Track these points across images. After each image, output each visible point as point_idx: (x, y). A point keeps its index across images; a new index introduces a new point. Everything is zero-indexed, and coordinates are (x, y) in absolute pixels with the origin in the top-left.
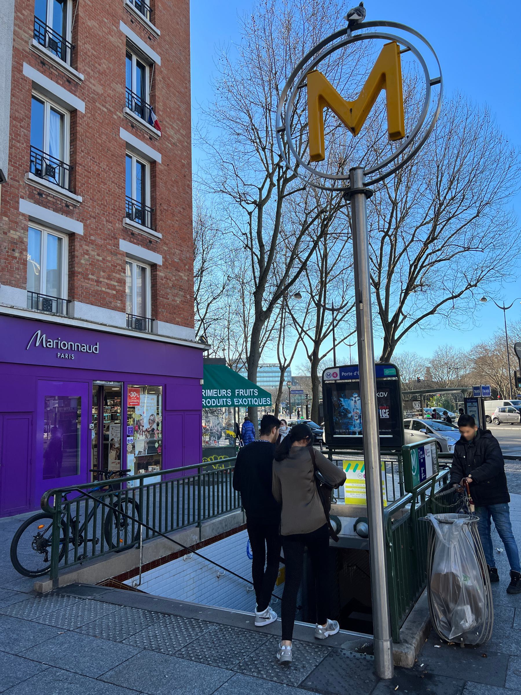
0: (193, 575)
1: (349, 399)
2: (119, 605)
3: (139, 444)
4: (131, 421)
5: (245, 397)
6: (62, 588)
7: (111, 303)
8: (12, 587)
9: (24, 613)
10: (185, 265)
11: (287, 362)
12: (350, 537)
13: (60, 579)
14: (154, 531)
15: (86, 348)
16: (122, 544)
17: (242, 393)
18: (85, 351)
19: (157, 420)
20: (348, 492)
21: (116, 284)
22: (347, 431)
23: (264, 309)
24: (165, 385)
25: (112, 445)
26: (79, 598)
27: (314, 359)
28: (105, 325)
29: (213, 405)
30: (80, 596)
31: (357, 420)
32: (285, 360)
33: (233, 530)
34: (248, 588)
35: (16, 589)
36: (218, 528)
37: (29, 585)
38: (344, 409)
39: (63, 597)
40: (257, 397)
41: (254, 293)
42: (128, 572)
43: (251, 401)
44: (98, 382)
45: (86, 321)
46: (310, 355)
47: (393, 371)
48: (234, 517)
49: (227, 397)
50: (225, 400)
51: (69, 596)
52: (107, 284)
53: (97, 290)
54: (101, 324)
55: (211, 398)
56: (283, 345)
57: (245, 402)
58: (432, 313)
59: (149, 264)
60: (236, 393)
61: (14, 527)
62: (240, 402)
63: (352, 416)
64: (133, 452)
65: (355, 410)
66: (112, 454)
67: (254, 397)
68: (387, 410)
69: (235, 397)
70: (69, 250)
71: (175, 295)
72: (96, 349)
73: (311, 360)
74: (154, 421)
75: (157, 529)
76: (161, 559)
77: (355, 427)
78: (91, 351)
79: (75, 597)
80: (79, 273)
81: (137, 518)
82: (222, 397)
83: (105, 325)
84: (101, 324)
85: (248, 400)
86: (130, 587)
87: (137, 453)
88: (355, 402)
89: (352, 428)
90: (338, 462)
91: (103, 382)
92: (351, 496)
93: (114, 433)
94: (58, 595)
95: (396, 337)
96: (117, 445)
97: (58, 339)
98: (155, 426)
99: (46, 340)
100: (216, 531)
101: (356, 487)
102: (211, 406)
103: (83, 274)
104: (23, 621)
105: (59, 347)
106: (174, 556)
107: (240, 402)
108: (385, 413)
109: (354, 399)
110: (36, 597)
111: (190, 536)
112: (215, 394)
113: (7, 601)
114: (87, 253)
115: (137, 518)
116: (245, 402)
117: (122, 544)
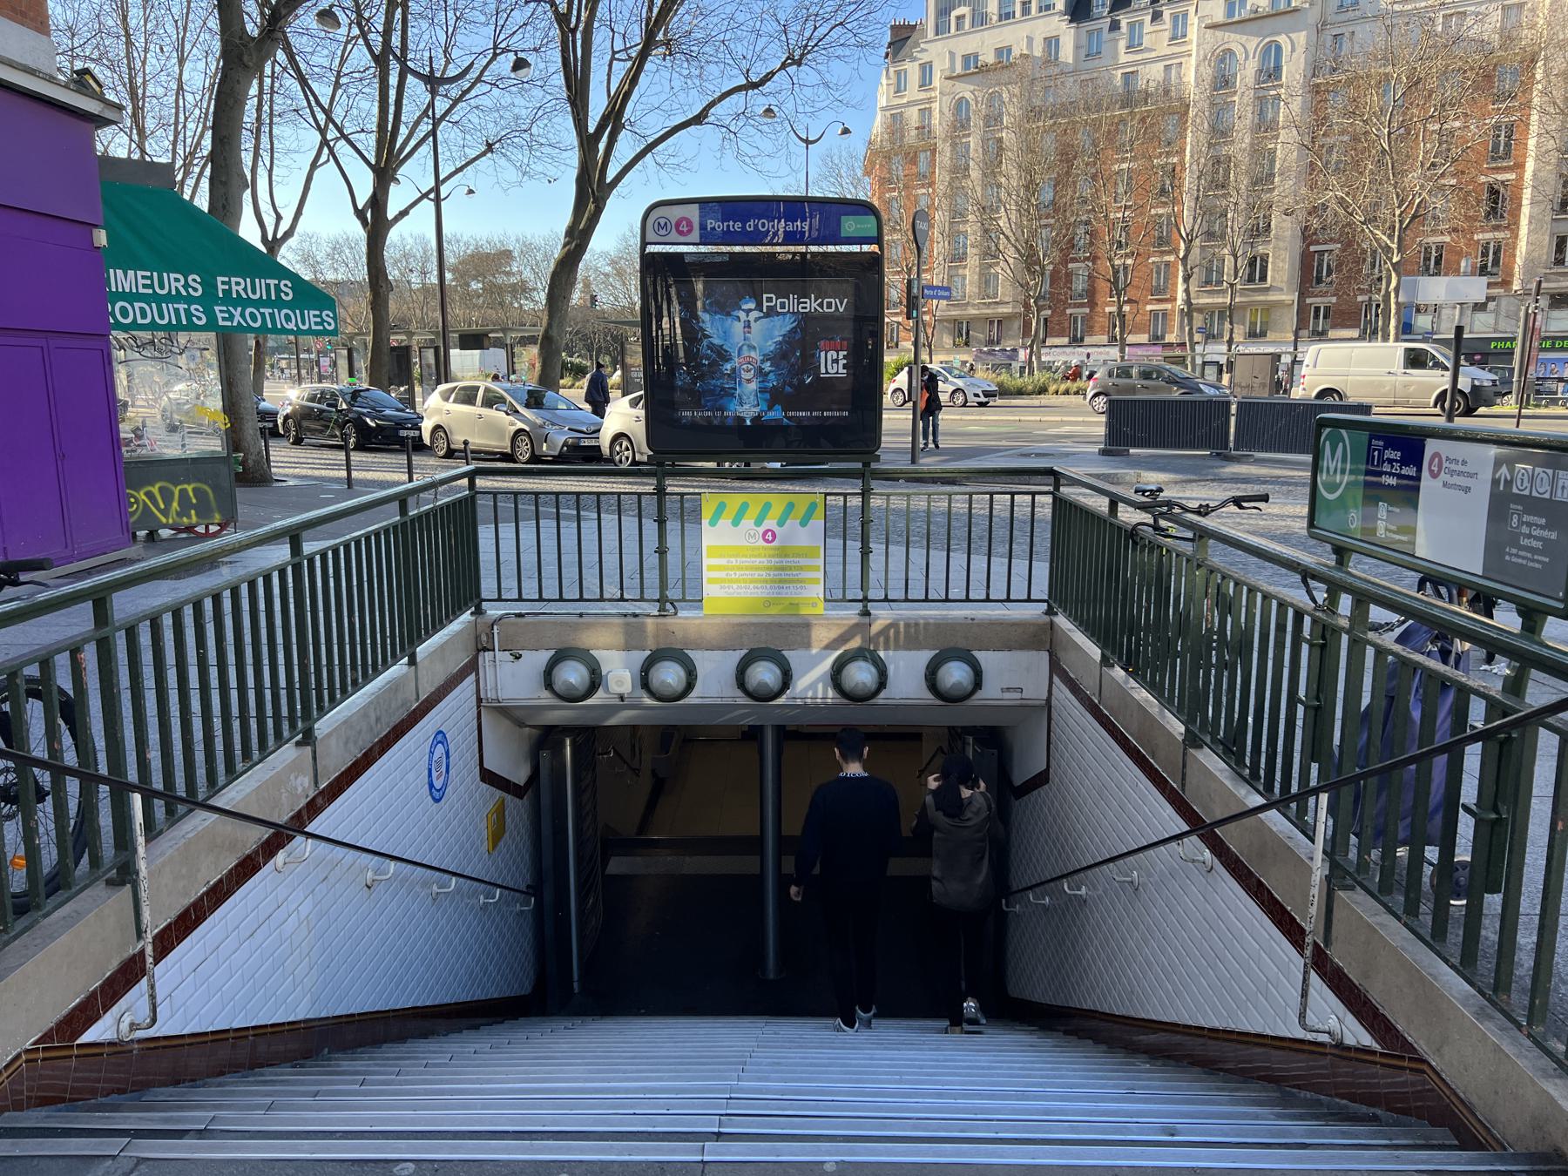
1: (728, 314)
5: (249, 302)
11: (284, 226)
12: (719, 701)
17: (240, 288)
20: (712, 581)
22: (719, 414)
27: (375, 219)
29: (140, 321)
31: (749, 381)
32: (279, 218)
33: (395, 728)
34: (435, 888)
36: (360, 732)
38: (711, 347)
40: (290, 305)
42: (94, 992)
43: (272, 315)
46: (360, 207)
49: (189, 300)
50: (182, 307)
55: (132, 297)
56: (270, 171)
57: (254, 319)
60: (221, 287)
62: (237, 318)
63: (734, 370)
65: (745, 352)
67: (279, 304)
68: (842, 354)
69: (216, 300)
73: (364, 222)
76: (207, 893)
77: (741, 404)
81: (70, 758)
82: (169, 298)
85: (263, 315)
86: (111, 1044)
88: (748, 325)
89: (732, 407)
90: (602, 498)
92: (722, 594)
100: (355, 743)
101: (740, 568)
102: (135, 325)
106: (247, 868)
107: (237, 318)
108: (836, 361)
109: (742, 315)
111: (272, 780)
112: (144, 286)
115: (70, 758)
116: (255, 320)
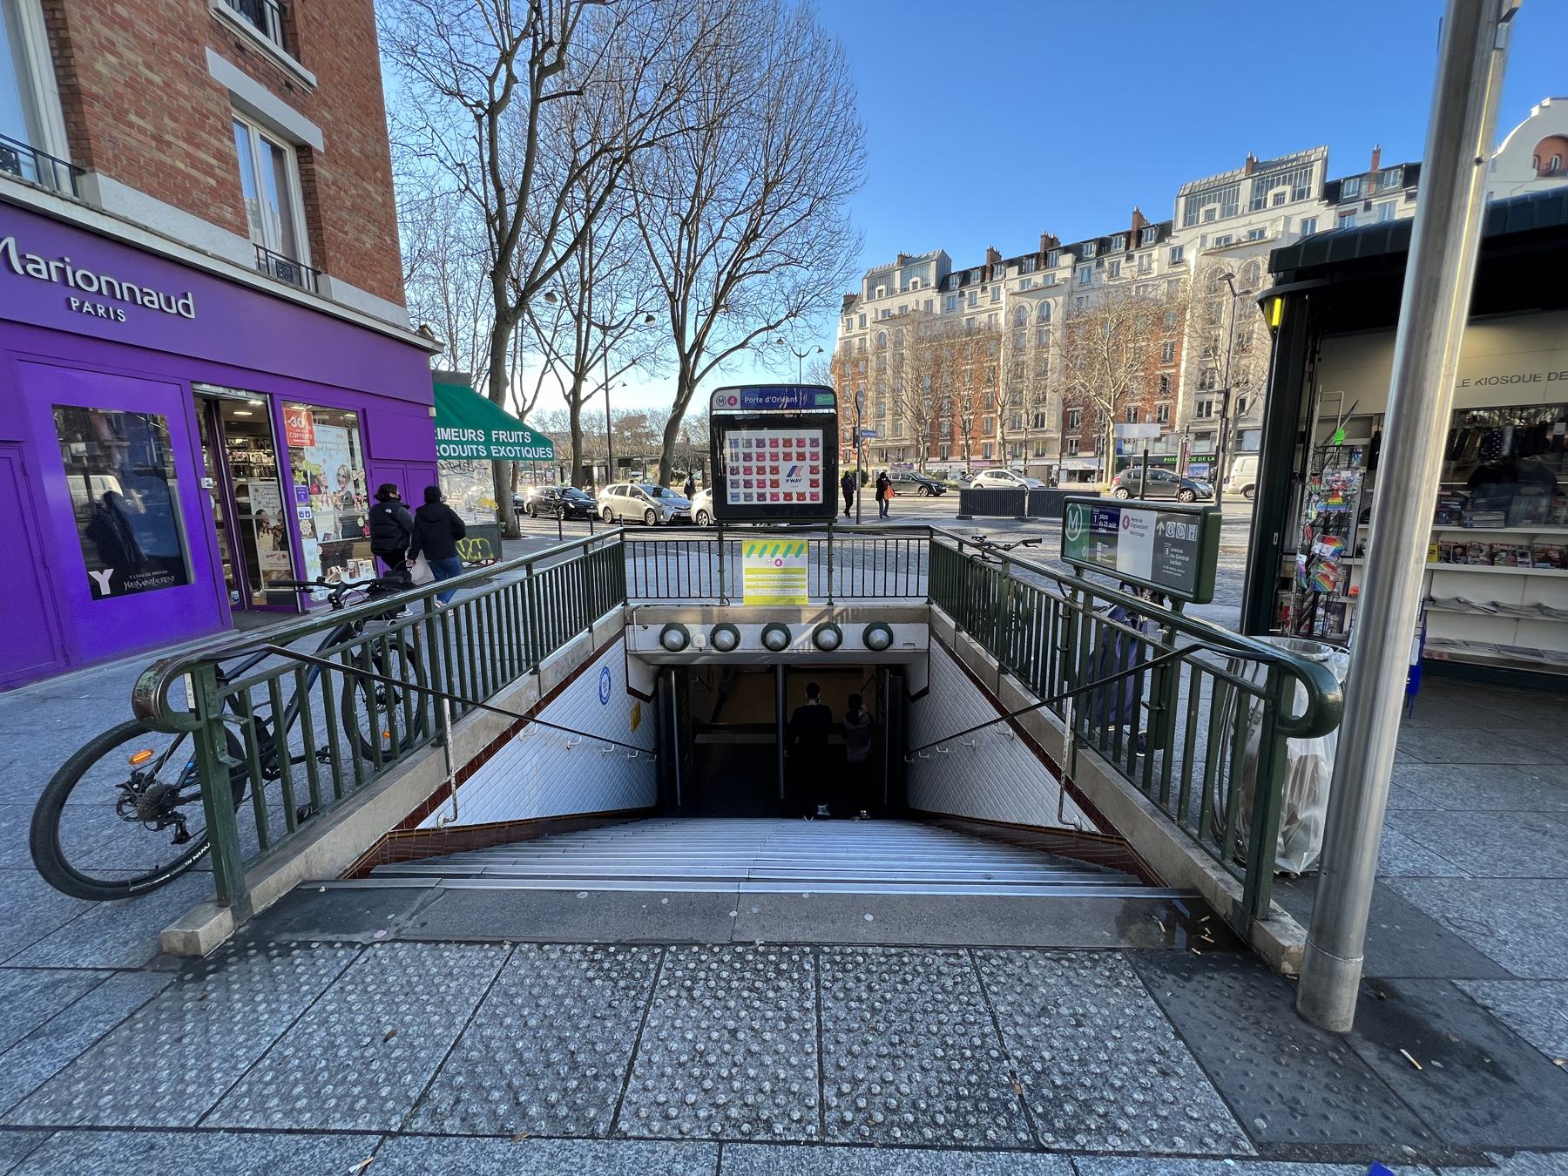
0: (534, 761)
2: (492, 943)
3: (322, 519)
4: (298, 478)
5: (508, 444)
6: (269, 912)
7: (207, 205)
8: (68, 953)
9: (154, 1083)
10: (375, 170)
13: (255, 893)
14: (465, 703)
15: (156, 300)
16: (385, 745)
18: (156, 306)
19: (355, 475)
21: (214, 162)
23: (511, 303)
24: (364, 411)
25: (260, 524)
26: (345, 944)
27: (575, 400)
28: (204, 253)
30: (345, 938)
35: (90, 958)
37: (136, 927)
39: (285, 951)
41: (492, 273)
44: (206, 387)
45: (146, 229)
47: (829, 399)
48: (581, 644)
49: (478, 443)
51: (306, 945)
52: (188, 155)
53: (163, 164)
54: (191, 248)
58: (742, 345)
59: (291, 143)
61: (26, 720)
64: (314, 534)
66: (265, 543)
67: (524, 444)
70: (46, 21)
71: (362, 230)
72: (188, 305)
74: (347, 477)
75: (458, 694)
78: (174, 311)
79: (331, 944)
80: (96, 97)
82: (467, 443)
83: (204, 253)
84: (191, 248)
87: (320, 536)
91: (221, 390)
93: (262, 498)
94: (263, 949)
95: (696, 375)
96: (273, 523)
97: (62, 260)
98: (350, 488)
99: (22, 257)
102: (450, 457)
103: (107, 106)
104: (161, 1139)
105: (71, 283)
106: (504, 738)
110: (181, 980)
111: (518, 692)
113: (59, 1033)
114: (109, 47)
117: (385, 745)
